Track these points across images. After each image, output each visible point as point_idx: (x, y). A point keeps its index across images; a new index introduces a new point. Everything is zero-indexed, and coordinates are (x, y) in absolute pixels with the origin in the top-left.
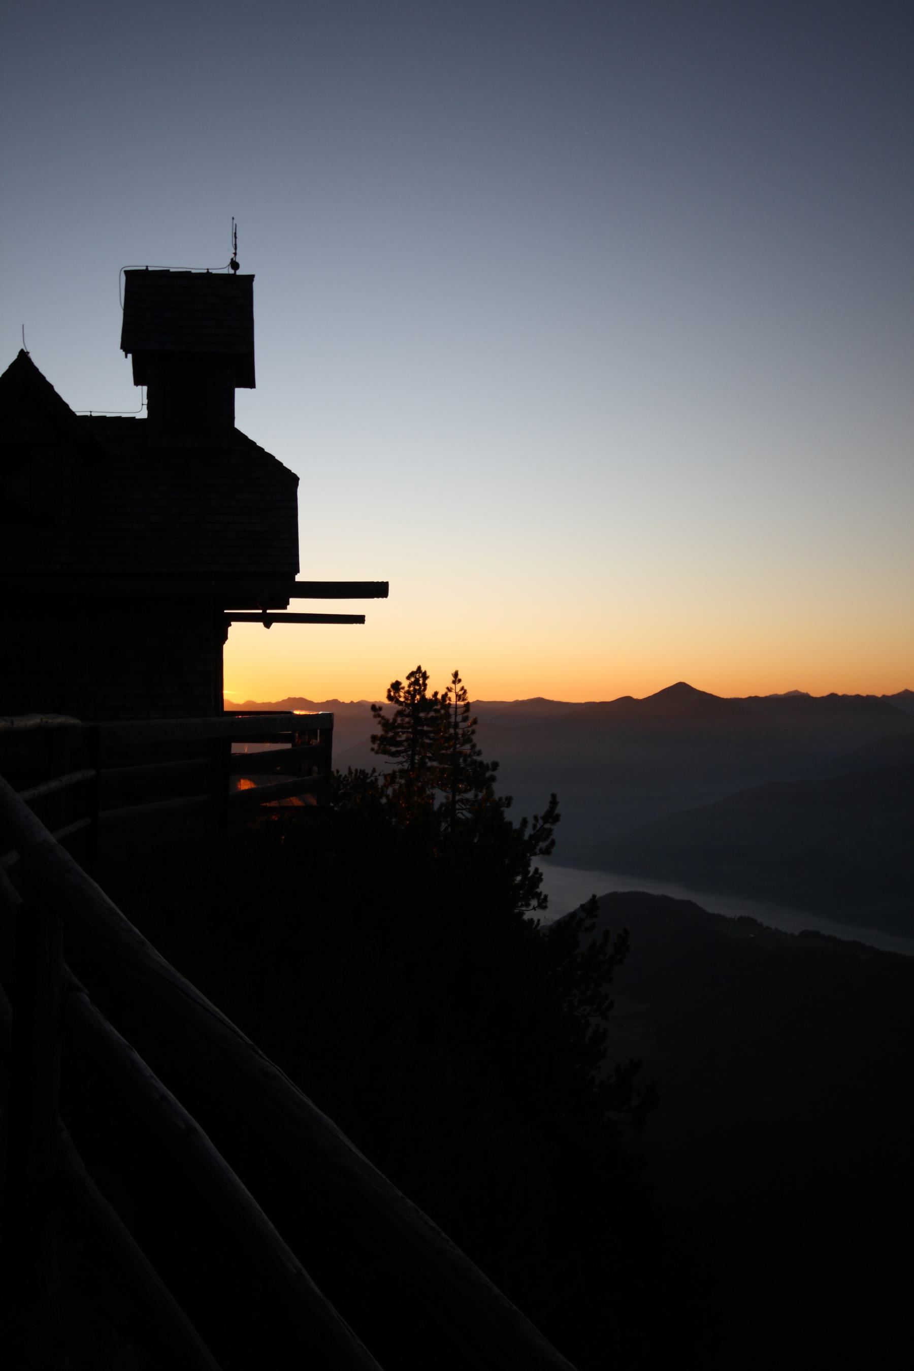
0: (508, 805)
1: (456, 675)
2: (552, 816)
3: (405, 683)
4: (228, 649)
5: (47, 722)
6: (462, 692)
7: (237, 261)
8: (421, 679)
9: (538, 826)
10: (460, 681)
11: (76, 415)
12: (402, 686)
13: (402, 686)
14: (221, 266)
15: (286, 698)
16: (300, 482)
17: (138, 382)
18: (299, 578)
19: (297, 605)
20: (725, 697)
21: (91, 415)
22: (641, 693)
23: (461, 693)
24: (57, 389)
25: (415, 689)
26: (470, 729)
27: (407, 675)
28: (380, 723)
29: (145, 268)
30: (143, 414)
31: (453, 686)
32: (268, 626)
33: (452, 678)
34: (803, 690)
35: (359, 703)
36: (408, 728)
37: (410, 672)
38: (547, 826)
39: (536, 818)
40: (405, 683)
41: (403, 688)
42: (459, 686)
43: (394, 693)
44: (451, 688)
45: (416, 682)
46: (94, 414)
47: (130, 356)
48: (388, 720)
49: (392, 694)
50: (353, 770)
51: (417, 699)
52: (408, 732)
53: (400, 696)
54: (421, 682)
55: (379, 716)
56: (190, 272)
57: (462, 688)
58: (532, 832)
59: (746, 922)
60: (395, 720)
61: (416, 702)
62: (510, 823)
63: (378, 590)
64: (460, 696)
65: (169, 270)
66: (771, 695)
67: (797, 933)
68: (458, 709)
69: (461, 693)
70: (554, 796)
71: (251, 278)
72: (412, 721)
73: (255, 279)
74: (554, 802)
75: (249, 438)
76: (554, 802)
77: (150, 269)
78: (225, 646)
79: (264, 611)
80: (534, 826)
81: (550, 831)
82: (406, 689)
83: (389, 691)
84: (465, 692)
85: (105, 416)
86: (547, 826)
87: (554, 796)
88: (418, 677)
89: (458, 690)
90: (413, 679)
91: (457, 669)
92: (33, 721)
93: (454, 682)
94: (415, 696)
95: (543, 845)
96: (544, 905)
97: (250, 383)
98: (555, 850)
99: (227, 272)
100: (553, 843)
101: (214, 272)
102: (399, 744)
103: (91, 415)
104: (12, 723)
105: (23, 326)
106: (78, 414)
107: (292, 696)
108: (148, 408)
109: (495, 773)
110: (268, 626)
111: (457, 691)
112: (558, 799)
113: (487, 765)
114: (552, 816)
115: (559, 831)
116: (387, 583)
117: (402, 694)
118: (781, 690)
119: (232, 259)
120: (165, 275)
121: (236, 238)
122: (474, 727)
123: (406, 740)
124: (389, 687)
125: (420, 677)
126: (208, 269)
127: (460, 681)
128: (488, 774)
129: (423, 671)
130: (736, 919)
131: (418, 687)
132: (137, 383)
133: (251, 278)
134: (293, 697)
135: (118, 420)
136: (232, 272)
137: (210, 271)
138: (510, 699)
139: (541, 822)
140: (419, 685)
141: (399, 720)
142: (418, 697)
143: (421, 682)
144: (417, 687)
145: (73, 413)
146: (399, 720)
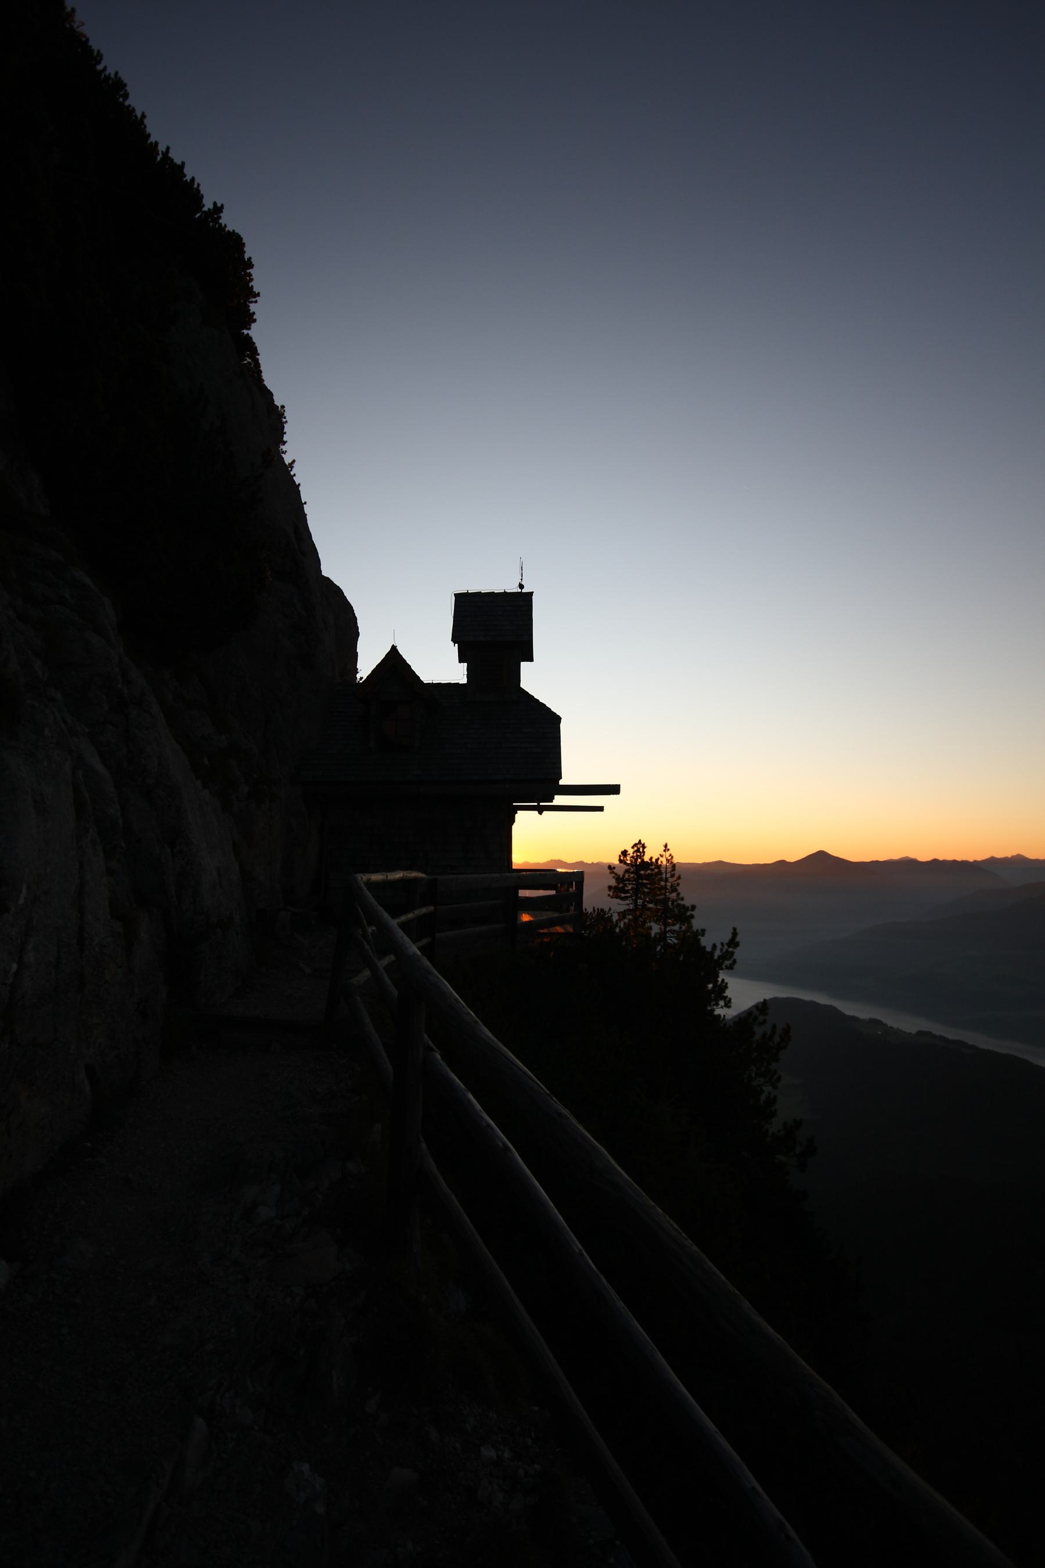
0: (703, 935)
1: (666, 846)
2: (733, 943)
3: (631, 851)
6: (670, 857)
9: (724, 950)
10: (668, 850)
12: (628, 853)
13: (628, 853)
15: (549, 860)
17: (461, 660)
18: (561, 782)
19: (559, 800)
22: (792, 857)
23: (670, 858)
26: (676, 883)
28: (614, 877)
29: (466, 591)
31: (664, 853)
32: (540, 813)
34: (912, 856)
35: (597, 863)
36: (633, 881)
38: (731, 949)
39: (722, 944)
40: (631, 851)
41: (629, 854)
42: (668, 853)
45: (638, 850)
46: (434, 682)
47: (456, 645)
48: (619, 876)
49: (622, 858)
50: (596, 909)
52: (633, 884)
53: (627, 860)
54: (641, 850)
55: (613, 873)
57: (670, 855)
58: (720, 954)
59: (875, 1022)
60: (624, 876)
63: (613, 790)
66: (903, 858)
67: (914, 1032)
69: (670, 858)
70: (735, 929)
71: (531, 593)
74: (735, 933)
76: (735, 933)
77: (469, 592)
78: (513, 827)
79: (539, 804)
80: (721, 950)
82: (631, 855)
83: (620, 856)
86: (731, 949)
90: (636, 848)
93: (665, 851)
94: (637, 860)
95: (727, 963)
97: (530, 659)
98: (736, 967)
100: (735, 961)
101: (508, 591)
102: (627, 892)
105: (600, 809)
106: (425, 682)
110: (540, 813)
114: (733, 943)
116: (619, 785)
117: (628, 858)
120: (478, 595)
122: (679, 881)
123: (631, 890)
124: (620, 854)
128: (689, 913)
132: (460, 662)
133: (531, 593)
136: (520, 590)
138: (700, 861)
139: (726, 947)
140: (640, 852)
141: (627, 876)
142: (639, 860)
143: (641, 850)
144: (639, 854)
145: (422, 682)
146: (627, 876)
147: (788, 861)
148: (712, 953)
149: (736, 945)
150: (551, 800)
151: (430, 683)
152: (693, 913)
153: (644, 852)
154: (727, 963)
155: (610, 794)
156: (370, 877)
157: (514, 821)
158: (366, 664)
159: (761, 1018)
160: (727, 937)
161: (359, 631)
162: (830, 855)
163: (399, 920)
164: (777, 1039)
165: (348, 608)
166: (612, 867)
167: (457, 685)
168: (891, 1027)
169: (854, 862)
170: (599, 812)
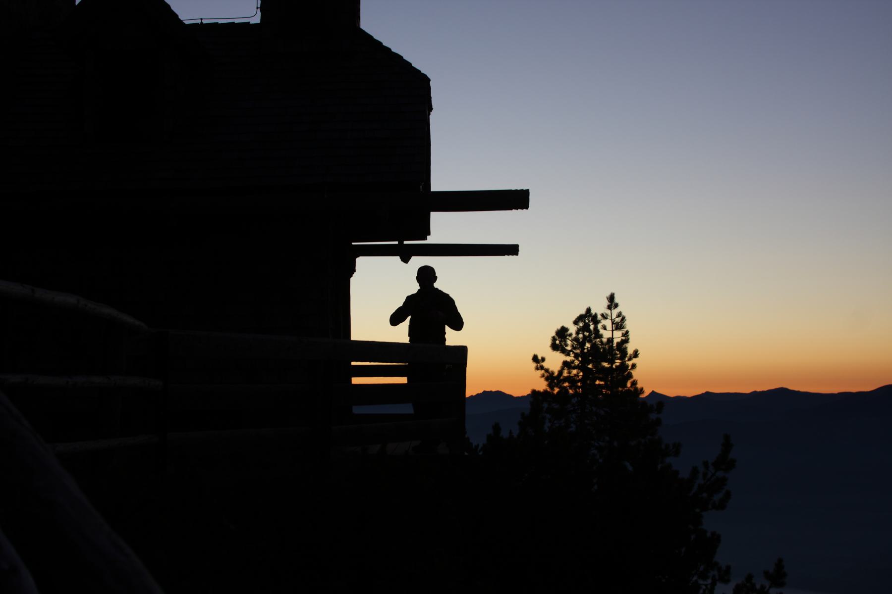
1: (611, 298)
2: (724, 462)
3: (573, 329)
4: (355, 282)
6: (620, 318)
10: (616, 306)
11: (184, 23)
12: (569, 332)
13: (569, 332)
16: (432, 84)
21: (202, 23)
28: (543, 376)
30: (256, 20)
31: (608, 312)
32: (406, 260)
33: (606, 303)
38: (720, 474)
39: (706, 464)
40: (573, 329)
41: (570, 335)
42: (615, 312)
43: (560, 342)
44: (606, 314)
45: (586, 328)
46: (205, 22)
48: (553, 373)
49: (557, 342)
51: (588, 348)
53: (567, 345)
54: (592, 327)
55: (542, 368)
57: (619, 315)
60: (560, 372)
64: (617, 323)
68: (614, 339)
72: (581, 374)
74: (727, 445)
75: (374, 38)
76: (727, 445)
78: (352, 279)
79: (401, 242)
82: (574, 335)
83: (554, 339)
84: (623, 319)
86: (720, 474)
88: (587, 321)
89: (614, 316)
90: (581, 324)
91: (613, 292)
92: (107, 311)
93: (609, 307)
95: (717, 498)
97: (249, 22)
100: (728, 495)
103: (202, 23)
105: (512, 250)
106: (187, 22)
107: (503, 391)
108: (261, 11)
110: (406, 260)
111: (613, 318)
114: (724, 462)
116: (527, 192)
117: (569, 342)
124: (554, 334)
125: (589, 321)
127: (616, 306)
128: (653, 416)
129: (594, 314)
131: (588, 333)
138: (747, 390)
140: (589, 331)
141: (565, 374)
142: (588, 345)
144: (587, 334)
145: (181, 22)
146: (565, 374)
150: (426, 232)
151: (198, 24)
155: (511, 209)
161: (506, 256)
166: (540, 358)
167: (245, 27)
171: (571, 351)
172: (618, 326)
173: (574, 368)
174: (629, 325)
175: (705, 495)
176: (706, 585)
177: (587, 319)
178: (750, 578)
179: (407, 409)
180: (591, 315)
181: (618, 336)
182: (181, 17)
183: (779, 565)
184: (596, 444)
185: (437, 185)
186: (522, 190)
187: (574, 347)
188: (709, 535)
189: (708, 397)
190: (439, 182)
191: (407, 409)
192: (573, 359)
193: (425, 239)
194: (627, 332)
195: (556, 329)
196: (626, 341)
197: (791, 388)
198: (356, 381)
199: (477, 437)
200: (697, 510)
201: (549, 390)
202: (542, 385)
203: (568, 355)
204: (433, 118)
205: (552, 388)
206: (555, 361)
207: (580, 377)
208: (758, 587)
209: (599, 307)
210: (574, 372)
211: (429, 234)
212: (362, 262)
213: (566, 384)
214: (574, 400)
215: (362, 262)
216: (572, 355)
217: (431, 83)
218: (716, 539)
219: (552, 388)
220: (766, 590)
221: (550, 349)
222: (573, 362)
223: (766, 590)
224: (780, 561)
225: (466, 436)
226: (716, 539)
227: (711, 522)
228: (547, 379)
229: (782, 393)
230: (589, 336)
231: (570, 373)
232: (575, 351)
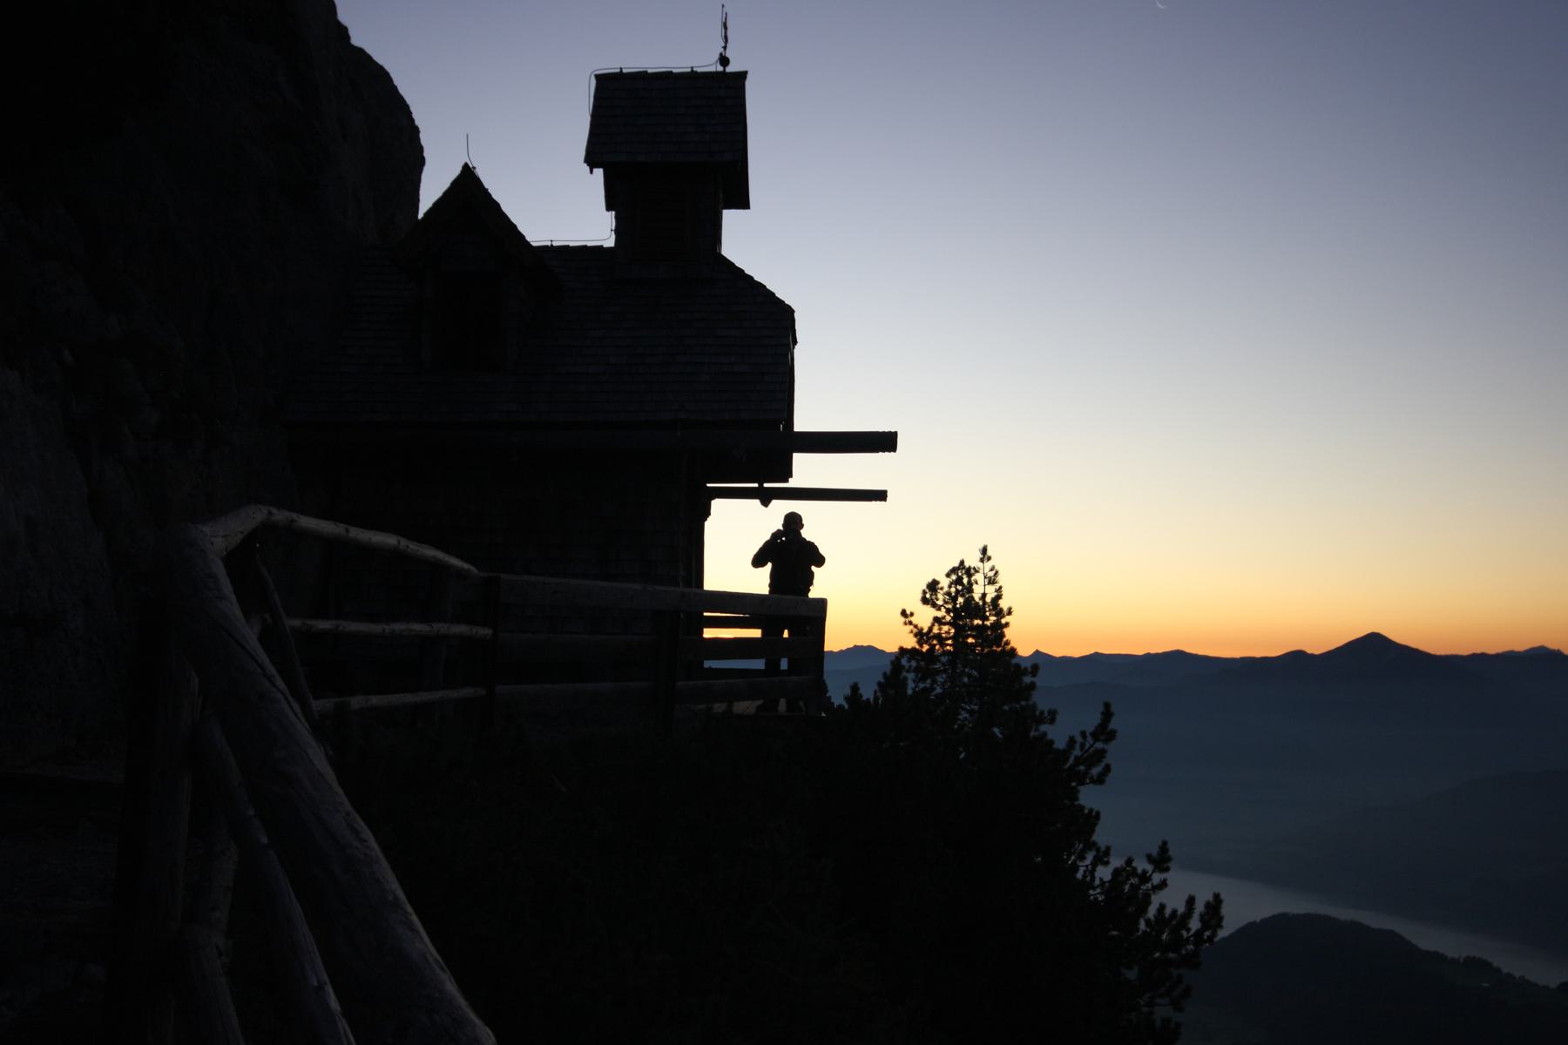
0: (1052, 721)
1: (984, 551)
2: (1104, 732)
3: (944, 583)
4: (710, 526)
5: (408, 547)
6: (993, 572)
7: (727, 56)
8: (964, 576)
9: (1087, 746)
10: (989, 558)
12: (940, 586)
14: (707, 63)
17: (609, 208)
19: (808, 469)
20: (1438, 652)
21: (552, 245)
24: (505, 208)
25: (957, 591)
27: (946, 572)
29: (618, 70)
30: (610, 242)
32: (765, 503)
37: (951, 568)
38: (1099, 745)
39: (1083, 734)
40: (944, 583)
41: (942, 589)
42: (988, 565)
43: (931, 595)
45: (959, 581)
46: (555, 244)
53: (937, 599)
54: (965, 580)
55: (911, 623)
56: (671, 72)
58: (1080, 754)
59: (1477, 965)
60: (930, 629)
61: (958, 606)
62: (1052, 742)
63: (884, 442)
64: (990, 578)
65: (646, 72)
67: (1553, 985)
69: (992, 574)
70: (1107, 706)
71: (742, 76)
72: (953, 631)
73: (748, 76)
74: (1107, 714)
76: (1107, 714)
77: (624, 71)
78: (706, 523)
80: (1082, 746)
81: (1101, 754)
82: (946, 589)
83: (924, 592)
85: (568, 246)
86: (1099, 745)
87: (1107, 706)
88: (960, 574)
89: (987, 570)
90: (954, 577)
92: (430, 552)
93: (982, 560)
95: (1095, 771)
96: (1106, 859)
97: (742, 202)
98: (1109, 779)
99: (714, 70)
100: (1107, 769)
101: (699, 70)
103: (552, 245)
104: (347, 531)
105: (880, 496)
106: (534, 244)
107: (859, 644)
108: (615, 233)
109: (1034, 679)
110: (765, 503)
112: (1113, 709)
113: (1026, 669)
114: (1104, 732)
115: (1114, 753)
117: (940, 596)
118: (1521, 645)
119: (721, 54)
120: (642, 77)
121: (726, 28)
124: (925, 587)
126: (692, 68)
129: (967, 566)
130: (1461, 960)
133: (742, 76)
134: (860, 645)
135: (584, 250)
136: (720, 69)
137: (695, 69)
138: (1140, 652)
139: (1090, 740)
140: (962, 584)
141: (936, 630)
142: (961, 600)
144: (959, 588)
145: (528, 243)
147: (1309, 651)
148: (1065, 754)
149: (1111, 736)
150: (786, 474)
151: (547, 246)
152: (1034, 679)
153: (971, 584)
154: (1095, 771)
155: (878, 452)
156: (296, 518)
157: (709, 514)
158: (432, 188)
159: (1157, 878)
160: (1091, 721)
162: (1394, 643)
163: (386, 627)
164: (1195, 924)
165: (400, 109)
166: (908, 612)
167: (599, 250)
168: (1509, 975)
169: (1440, 657)
170: (878, 502)
171: (942, 606)
172: (992, 581)
173: (945, 624)
174: (1002, 580)
175: (1082, 768)
176: (1087, 866)
177: (961, 573)
178: (1129, 862)
179: (758, 664)
180: (964, 568)
181: (991, 593)
182: (528, 239)
183: (1164, 848)
184: (969, 708)
185: (799, 426)
186: (890, 432)
187: (946, 603)
188: (1086, 811)
189: (1096, 660)
190: (803, 421)
191: (758, 664)
192: (945, 614)
193: (787, 481)
194: (1001, 588)
195: (927, 582)
196: (999, 597)
197: (1188, 650)
198: (709, 633)
199: (838, 695)
200: (1074, 784)
201: (917, 647)
202: (910, 642)
203: (939, 609)
204: (799, 352)
205: (921, 646)
206: (925, 617)
207: (952, 634)
208: (1139, 871)
209: (972, 561)
210: (945, 628)
211: (791, 477)
212: (717, 505)
213: (935, 642)
214: (944, 659)
215: (717, 505)
216: (943, 610)
217: (796, 315)
218: (1093, 818)
219: (921, 646)
220: (1148, 875)
221: (920, 603)
222: (944, 618)
223: (1148, 875)
224: (1165, 843)
225: (828, 695)
226: (1093, 818)
227: (1088, 797)
228: (916, 635)
229: (1177, 659)
230: (962, 590)
231: (940, 629)
232: (947, 606)
